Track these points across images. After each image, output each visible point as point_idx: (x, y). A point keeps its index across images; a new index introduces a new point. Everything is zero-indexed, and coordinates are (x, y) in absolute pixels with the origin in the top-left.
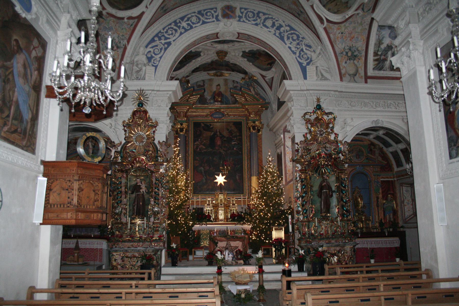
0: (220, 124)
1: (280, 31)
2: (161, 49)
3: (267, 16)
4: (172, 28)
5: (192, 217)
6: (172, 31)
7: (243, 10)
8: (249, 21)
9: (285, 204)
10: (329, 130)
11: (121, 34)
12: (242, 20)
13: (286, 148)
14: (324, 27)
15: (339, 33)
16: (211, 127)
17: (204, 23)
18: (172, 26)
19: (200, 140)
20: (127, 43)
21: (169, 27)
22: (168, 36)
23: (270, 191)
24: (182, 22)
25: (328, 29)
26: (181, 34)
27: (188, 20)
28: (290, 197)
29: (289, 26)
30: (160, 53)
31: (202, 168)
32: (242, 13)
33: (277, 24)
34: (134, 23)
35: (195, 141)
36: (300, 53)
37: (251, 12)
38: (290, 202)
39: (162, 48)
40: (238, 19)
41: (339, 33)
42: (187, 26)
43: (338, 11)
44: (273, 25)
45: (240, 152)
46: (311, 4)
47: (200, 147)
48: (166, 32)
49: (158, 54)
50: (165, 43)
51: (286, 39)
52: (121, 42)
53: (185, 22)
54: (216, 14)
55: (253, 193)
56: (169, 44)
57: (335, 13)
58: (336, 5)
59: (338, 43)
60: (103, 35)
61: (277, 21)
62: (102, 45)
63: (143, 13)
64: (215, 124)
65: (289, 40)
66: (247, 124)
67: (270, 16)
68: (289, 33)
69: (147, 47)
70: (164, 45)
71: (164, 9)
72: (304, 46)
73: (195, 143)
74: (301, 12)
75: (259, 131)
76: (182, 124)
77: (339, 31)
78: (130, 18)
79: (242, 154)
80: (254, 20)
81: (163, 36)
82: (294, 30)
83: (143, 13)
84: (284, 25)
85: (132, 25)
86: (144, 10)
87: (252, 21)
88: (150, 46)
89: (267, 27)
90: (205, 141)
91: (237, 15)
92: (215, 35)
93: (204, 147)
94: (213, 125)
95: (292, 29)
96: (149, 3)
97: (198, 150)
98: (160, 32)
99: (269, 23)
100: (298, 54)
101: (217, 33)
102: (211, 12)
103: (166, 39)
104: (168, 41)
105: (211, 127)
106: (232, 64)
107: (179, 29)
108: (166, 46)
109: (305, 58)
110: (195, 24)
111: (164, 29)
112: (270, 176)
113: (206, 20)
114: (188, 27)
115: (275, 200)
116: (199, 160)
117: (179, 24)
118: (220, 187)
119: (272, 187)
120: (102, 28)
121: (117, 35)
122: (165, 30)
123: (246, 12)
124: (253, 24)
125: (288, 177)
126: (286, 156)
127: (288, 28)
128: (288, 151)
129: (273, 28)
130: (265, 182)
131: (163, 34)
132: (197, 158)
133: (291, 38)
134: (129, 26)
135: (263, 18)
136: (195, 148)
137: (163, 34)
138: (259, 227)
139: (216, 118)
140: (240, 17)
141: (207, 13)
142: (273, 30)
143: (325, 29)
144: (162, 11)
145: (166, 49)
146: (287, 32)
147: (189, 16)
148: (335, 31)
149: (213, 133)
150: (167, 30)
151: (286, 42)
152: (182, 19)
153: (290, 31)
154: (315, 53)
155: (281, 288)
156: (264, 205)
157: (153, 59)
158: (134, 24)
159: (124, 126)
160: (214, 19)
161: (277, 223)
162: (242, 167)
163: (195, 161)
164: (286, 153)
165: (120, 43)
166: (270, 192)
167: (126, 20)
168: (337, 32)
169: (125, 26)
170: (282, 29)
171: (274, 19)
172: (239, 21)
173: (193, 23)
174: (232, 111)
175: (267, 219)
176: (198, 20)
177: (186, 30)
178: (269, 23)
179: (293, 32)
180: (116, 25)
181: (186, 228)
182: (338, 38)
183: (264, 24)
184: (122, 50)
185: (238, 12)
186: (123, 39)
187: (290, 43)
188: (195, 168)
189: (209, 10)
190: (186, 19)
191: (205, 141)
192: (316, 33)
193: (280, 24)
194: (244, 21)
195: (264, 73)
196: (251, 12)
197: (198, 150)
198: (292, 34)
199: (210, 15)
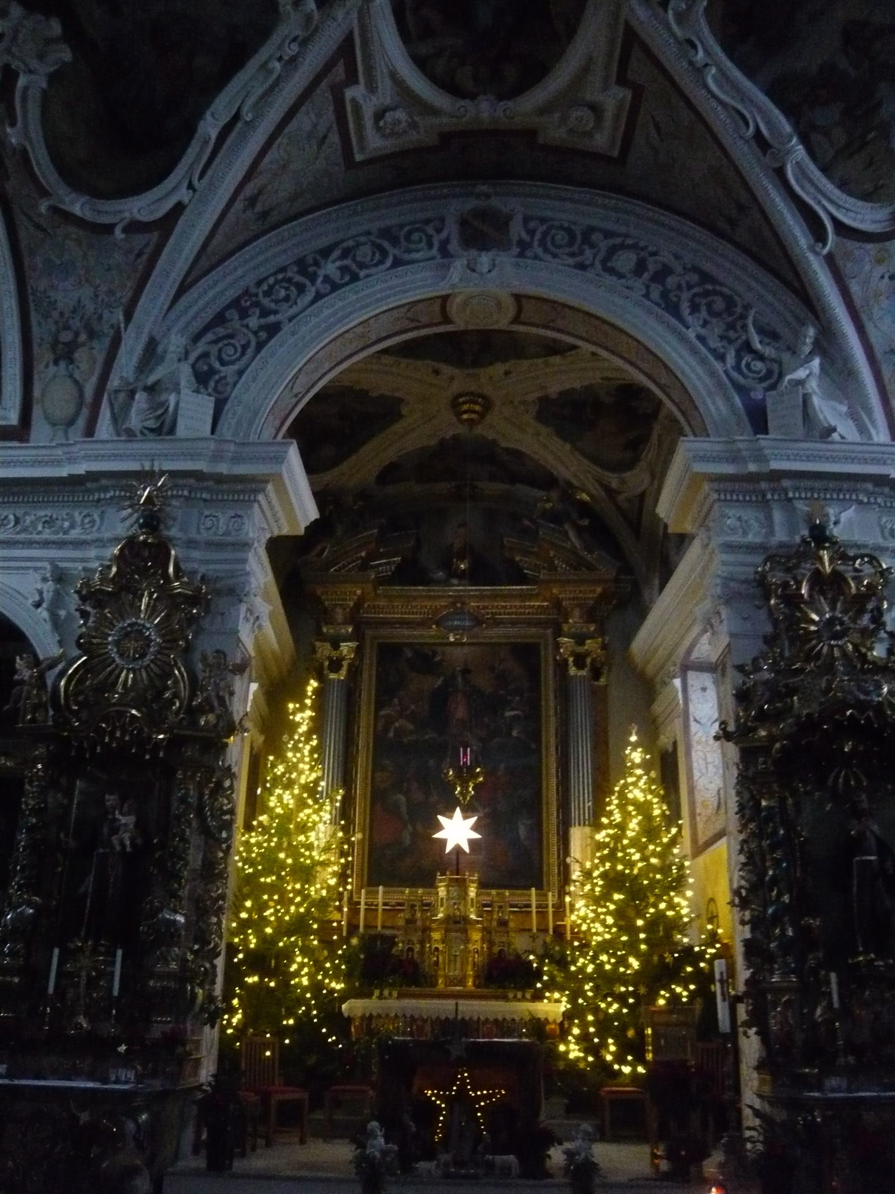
0: (466, 650)
1: (663, 285)
2: (244, 348)
3: (618, 241)
4: (289, 281)
5: (346, 963)
6: (287, 289)
7: (532, 224)
8: (555, 256)
9: (694, 924)
10: (865, 620)
11: (104, 288)
12: (529, 253)
13: (693, 724)
14: (825, 251)
15: (882, 277)
16: (438, 658)
17: (397, 263)
18: (290, 274)
19: (396, 700)
20: (121, 318)
21: (280, 276)
22: (273, 306)
23: (636, 871)
24: (322, 262)
25: (840, 263)
26: (319, 296)
27: (343, 257)
28: (712, 900)
29: (695, 269)
30: (238, 359)
31: (402, 798)
32: (531, 233)
33: (652, 266)
34: (147, 245)
35: (379, 705)
36: (739, 358)
37: (562, 228)
38: (712, 919)
39: (249, 342)
40: (516, 250)
41: (882, 277)
42: (338, 273)
43: (876, 188)
44: (640, 268)
45: (534, 746)
46: (777, 165)
47: (397, 725)
48: (267, 294)
49: (233, 363)
50: (262, 328)
51: (688, 311)
52: (105, 316)
53: (334, 262)
54: (444, 235)
55: (575, 881)
56: (273, 329)
57: (866, 197)
58: (871, 164)
59: (876, 312)
60: (41, 288)
61: (654, 254)
62: (40, 324)
63: (179, 208)
64: (448, 649)
65: (697, 315)
66: (557, 646)
67: (630, 242)
68: (696, 290)
69: (196, 338)
70: (255, 333)
71: (259, 208)
72: (752, 329)
73: (382, 713)
74: (741, 208)
75: (596, 673)
76: (336, 646)
77: (880, 270)
78: (134, 227)
79: (538, 751)
80: (572, 255)
81: (257, 304)
82: (714, 281)
83: (179, 208)
84: (679, 269)
85: (139, 255)
86: (183, 195)
87: (566, 257)
88: (210, 336)
89: (621, 276)
90: (413, 707)
91: (515, 238)
92: (437, 307)
93: (411, 727)
94: (443, 653)
95: (705, 277)
96: (197, 176)
97: (391, 734)
98: (246, 292)
99: (625, 261)
100: (731, 359)
101: (445, 299)
102: (424, 231)
103: (265, 313)
104: (272, 319)
105: (438, 658)
106: (508, 450)
107: (313, 284)
108: (263, 335)
109: (758, 373)
110: (367, 267)
111: (259, 284)
112: (635, 816)
113: (406, 257)
114: (342, 278)
115: (655, 906)
116: (390, 769)
117: (311, 269)
118: (454, 857)
119: (644, 858)
120: (40, 265)
121: (92, 290)
122: (265, 287)
123: (544, 227)
124: (569, 266)
125: (700, 826)
126: (693, 754)
127: (695, 278)
128: (700, 734)
129: (640, 276)
130: (617, 838)
131: (254, 299)
132: (387, 762)
133: (704, 309)
134: (132, 257)
135: (604, 245)
136: (380, 728)
137: (254, 299)
138: (596, 1010)
139: (453, 629)
140: (524, 246)
141: (410, 232)
142: (639, 285)
143: (830, 260)
144: (249, 213)
145: (260, 346)
146: (690, 287)
147: (351, 243)
148: (868, 267)
149: (442, 679)
150: (271, 287)
151: (690, 319)
152: (325, 253)
153: (701, 284)
154: (794, 353)
155: (767, 394)
156: (615, 925)
157: (217, 377)
158: (148, 250)
159: (83, 599)
160: (435, 252)
161: (663, 997)
162: (538, 794)
163: (379, 774)
164: (694, 744)
165: (100, 317)
166: (637, 876)
167: (118, 234)
168: (877, 274)
169: (118, 257)
170: (671, 281)
171: (644, 248)
172: (521, 255)
173: (362, 266)
174: (505, 607)
175: (623, 980)
176: (377, 256)
177: (335, 287)
178: (625, 261)
179: (709, 287)
180: (85, 254)
181: (316, 1007)
182: (877, 295)
183: (609, 264)
184: (107, 341)
185: (517, 230)
186: (109, 306)
187: (701, 322)
188: (377, 796)
189: (417, 226)
190: (337, 253)
191: (413, 707)
192: (796, 284)
193: (664, 265)
194: (536, 257)
195: (614, 481)
196: (562, 228)
197: (391, 734)
198: (706, 294)
199: (420, 241)
